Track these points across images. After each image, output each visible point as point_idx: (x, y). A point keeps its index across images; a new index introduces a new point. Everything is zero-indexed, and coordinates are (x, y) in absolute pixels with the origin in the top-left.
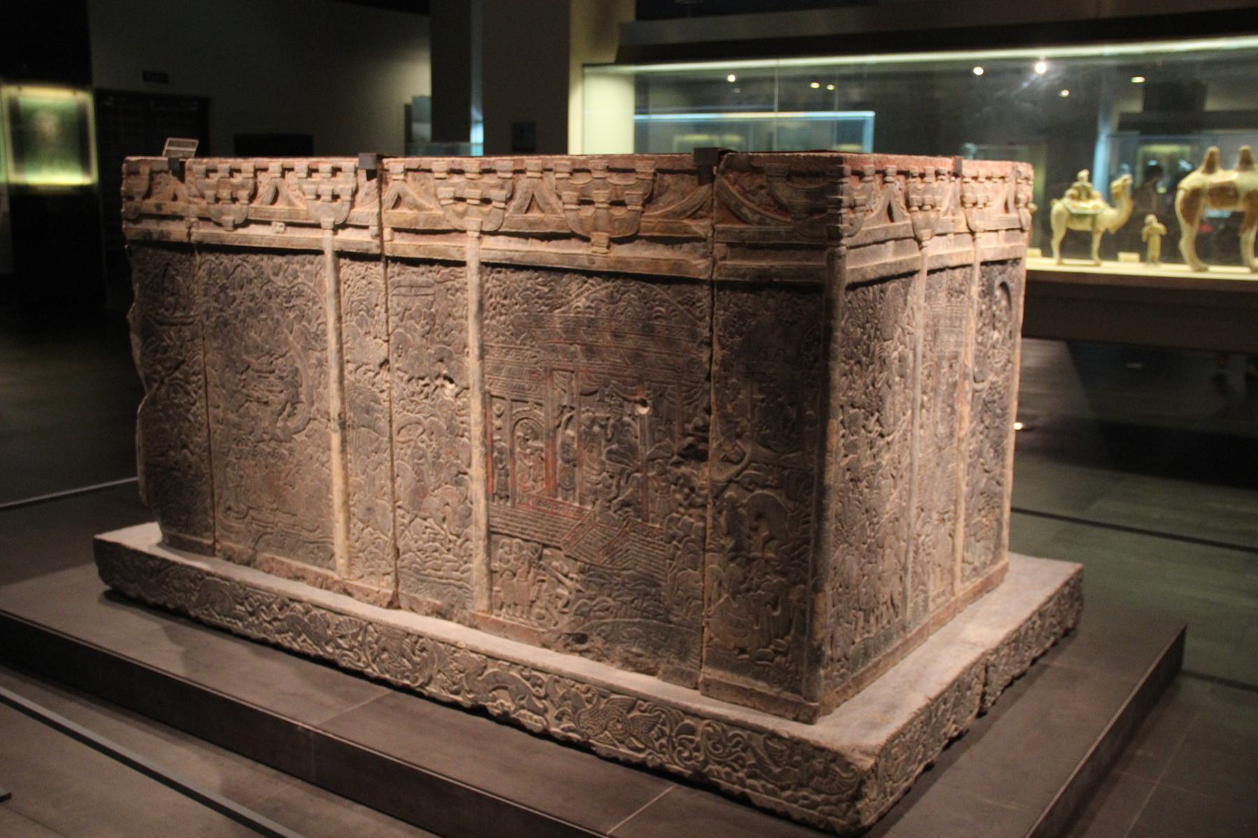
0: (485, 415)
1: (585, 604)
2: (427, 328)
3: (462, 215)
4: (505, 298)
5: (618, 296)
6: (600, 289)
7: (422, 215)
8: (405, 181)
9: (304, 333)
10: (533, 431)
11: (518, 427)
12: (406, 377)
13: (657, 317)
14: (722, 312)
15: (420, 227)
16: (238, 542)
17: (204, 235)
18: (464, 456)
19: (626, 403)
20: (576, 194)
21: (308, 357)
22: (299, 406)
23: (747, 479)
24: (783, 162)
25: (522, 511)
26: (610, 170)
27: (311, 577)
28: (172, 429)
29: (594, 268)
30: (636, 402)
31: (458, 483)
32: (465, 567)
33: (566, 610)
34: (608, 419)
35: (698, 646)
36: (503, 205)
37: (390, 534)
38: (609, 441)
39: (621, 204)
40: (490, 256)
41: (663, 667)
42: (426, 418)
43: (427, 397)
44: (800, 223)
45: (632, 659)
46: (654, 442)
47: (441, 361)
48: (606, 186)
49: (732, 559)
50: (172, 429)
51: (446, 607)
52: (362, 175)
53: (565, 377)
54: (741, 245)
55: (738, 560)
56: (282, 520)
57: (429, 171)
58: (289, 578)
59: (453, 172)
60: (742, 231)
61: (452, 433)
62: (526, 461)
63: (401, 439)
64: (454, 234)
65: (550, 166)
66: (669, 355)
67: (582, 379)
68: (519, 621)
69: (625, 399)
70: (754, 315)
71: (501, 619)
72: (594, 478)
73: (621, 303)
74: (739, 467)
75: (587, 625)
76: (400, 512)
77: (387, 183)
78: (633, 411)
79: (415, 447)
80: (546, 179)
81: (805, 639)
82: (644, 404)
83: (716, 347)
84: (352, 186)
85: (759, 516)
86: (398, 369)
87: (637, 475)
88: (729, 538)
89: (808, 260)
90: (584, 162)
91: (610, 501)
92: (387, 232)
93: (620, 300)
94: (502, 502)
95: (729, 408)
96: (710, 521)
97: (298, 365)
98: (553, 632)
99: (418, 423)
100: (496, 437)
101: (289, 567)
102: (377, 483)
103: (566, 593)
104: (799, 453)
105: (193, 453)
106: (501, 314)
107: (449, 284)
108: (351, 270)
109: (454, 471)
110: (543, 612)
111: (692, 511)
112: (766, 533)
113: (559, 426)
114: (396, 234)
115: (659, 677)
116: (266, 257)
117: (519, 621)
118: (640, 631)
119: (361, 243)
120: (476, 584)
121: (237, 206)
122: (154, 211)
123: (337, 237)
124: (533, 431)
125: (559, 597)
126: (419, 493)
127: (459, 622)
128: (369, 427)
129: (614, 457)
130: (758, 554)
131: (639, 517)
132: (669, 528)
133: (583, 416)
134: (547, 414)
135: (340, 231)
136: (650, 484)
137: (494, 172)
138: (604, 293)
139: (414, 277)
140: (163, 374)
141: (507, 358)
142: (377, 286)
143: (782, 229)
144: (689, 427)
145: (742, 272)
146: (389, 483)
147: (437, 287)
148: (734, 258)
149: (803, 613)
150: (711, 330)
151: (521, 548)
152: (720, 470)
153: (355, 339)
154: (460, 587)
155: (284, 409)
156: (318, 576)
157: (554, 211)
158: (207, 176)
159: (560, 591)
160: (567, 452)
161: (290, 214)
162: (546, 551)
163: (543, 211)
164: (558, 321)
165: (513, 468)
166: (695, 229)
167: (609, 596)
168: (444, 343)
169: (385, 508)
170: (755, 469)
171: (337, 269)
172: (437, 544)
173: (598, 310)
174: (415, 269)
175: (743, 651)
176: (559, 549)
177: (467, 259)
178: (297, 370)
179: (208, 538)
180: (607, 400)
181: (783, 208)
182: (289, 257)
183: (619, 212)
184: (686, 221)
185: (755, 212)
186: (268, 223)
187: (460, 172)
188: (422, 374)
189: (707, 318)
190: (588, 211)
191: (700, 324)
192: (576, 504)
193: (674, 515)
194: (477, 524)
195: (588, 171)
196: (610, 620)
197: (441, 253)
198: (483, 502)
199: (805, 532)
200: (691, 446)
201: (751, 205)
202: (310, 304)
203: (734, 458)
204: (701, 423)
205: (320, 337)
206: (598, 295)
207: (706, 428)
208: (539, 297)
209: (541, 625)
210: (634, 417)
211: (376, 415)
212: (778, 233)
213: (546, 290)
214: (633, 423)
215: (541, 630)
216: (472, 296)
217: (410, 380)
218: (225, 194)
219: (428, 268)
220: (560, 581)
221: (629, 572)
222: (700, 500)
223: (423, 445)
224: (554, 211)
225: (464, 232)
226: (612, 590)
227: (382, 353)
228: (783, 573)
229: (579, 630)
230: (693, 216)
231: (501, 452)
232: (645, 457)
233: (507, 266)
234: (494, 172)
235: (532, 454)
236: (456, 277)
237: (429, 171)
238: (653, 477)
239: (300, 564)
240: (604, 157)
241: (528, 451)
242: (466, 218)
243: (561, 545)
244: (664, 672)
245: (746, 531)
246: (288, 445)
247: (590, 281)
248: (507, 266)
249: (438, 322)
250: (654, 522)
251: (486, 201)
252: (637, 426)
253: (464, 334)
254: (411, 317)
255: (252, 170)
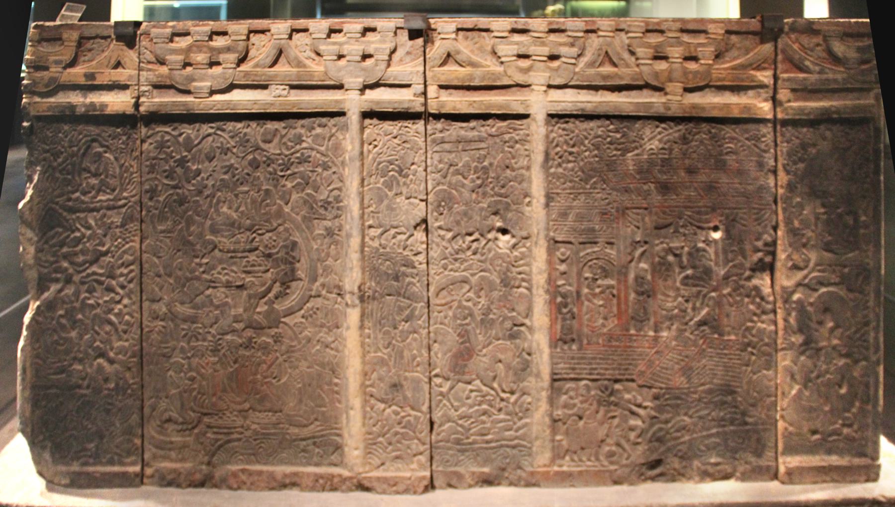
0: (549, 262)
1: (661, 429)
2: (479, 182)
3: (527, 71)
4: (573, 146)
5: (691, 137)
6: (674, 132)
7: (478, 72)
8: (456, 39)
9: (310, 203)
10: (604, 270)
11: (586, 268)
12: (449, 235)
13: (727, 153)
14: (785, 144)
15: (476, 83)
16: (183, 460)
17: (161, 104)
18: (521, 308)
19: (699, 231)
20: (652, 51)
21: (310, 229)
22: (294, 284)
23: (814, 281)
24: (838, 26)
25: (589, 353)
26: (683, 31)
27: (306, 481)
28: (81, 337)
29: (670, 113)
30: (709, 228)
31: (513, 337)
32: (519, 424)
33: (639, 440)
34: (682, 248)
35: (773, 440)
36: (573, 61)
37: (425, 408)
38: (683, 268)
39: (695, 59)
40: (559, 108)
41: (741, 469)
42: (473, 275)
43: (474, 253)
44: (852, 71)
45: (710, 469)
46: (727, 261)
47: (496, 213)
48: (680, 43)
49: (802, 353)
50: (81, 337)
51: (495, 472)
52: (404, 36)
53: (638, 214)
54: (802, 90)
55: (808, 353)
56: (259, 420)
57: (487, 30)
58: (272, 489)
59: (514, 31)
60: (805, 79)
61: (505, 286)
62: (595, 301)
63: (438, 302)
64: (514, 89)
65: (623, 26)
66: (740, 184)
67: (656, 214)
68: (589, 465)
69: (699, 227)
70: (814, 145)
71: (565, 468)
72: (669, 305)
73: (694, 143)
74: (805, 272)
75: (662, 449)
76: (438, 381)
77: (433, 43)
78: (707, 236)
79: (459, 307)
80: (617, 38)
81: (870, 407)
82: (716, 229)
83: (781, 174)
84: (389, 46)
85: (826, 310)
86: (440, 228)
87: (713, 294)
88: (798, 336)
89: (859, 99)
90: (658, 24)
91: (686, 324)
92: (432, 91)
93: (692, 141)
94: (566, 347)
95: (796, 224)
96: (781, 323)
97: (297, 237)
98: (626, 466)
99: (465, 281)
100: (560, 282)
101: (272, 476)
102: (406, 353)
103: (639, 423)
104: (857, 252)
105: (111, 362)
106: (569, 162)
107: (507, 137)
108: (375, 128)
109: (508, 324)
110: (614, 448)
111: (764, 317)
112: (831, 324)
113: (631, 261)
114: (443, 91)
115: (737, 479)
116: (254, 124)
117: (589, 465)
118: (718, 440)
119: (400, 102)
120: (537, 438)
121: (216, 70)
122: (82, 81)
123: (363, 97)
124: (604, 270)
125: (632, 429)
126: (463, 357)
127: (511, 484)
128: (399, 294)
129: (691, 281)
130: (824, 344)
131: (715, 332)
132: (744, 336)
133: (658, 248)
134: (618, 251)
135: (368, 91)
136: (725, 300)
137: (563, 31)
138: (676, 135)
139: (463, 132)
140: (71, 271)
141: (575, 203)
142: (416, 143)
143: (839, 77)
144: (760, 244)
145: (806, 112)
146: (425, 353)
147: (490, 141)
148: (796, 100)
149: (867, 385)
150: (776, 160)
151: (588, 388)
152: (788, 277)
153: (381, 201)
154: (514, 447)
155: (269, 290)
156: (317, 477)
157: (627, 66)
158: (172, 41)
159: (633, 422)
160: (641, 285)
161: (299, 76)
162: (617, 386)
163: (615, 65)
164: (630, 162)
165: (580, 310)
166: (761, 78)
167: (686, 414)
168: (501, 195)
169: (419, 381)
170: (819, 271)
171: (362, 129)
172: (485, 406)
173: (671, 150)
174: (464, 125)
175: (814, 432)
176: (633, 380)
177: (531, 111)
178: (295, 244)
179: (133, 464)
180: (682, 230)
181: (836, 59)
182: (291, 122)
183: (692, 66)
184: (752, 72)
185: (817, 64)
186: (265, 87)
187: (524, 31)
188: (471, 230)
189: (772, 151)
190: (662, 66)
191: (767, 155)
192: (651, 333)
193: (749, 324)
194: (538, 375)
195: (662, 32)
196: (687, 438)
197: (501, 107)
198: (546, 350)
199: (865, 316)
200: (761, 260)
201: (811, 59)
202: (319, 170)
203: (802, 264)
204: (769, 239)
205: (334, 205)
206: (671, 137)
207: (774, 243)
208: (610, 143)
209: (612, 463)
210: (707, 242)
211: (408, 280)
212: (835, 81)
213: (618, 136)
214: (708, 248)
215: (612, 467)
216: (538, 147)
217: (454, 237)
218: (201, 57)
219: (481, 122)
220: (633, 413)
221: (707, 386)
222: (770, 307)
223: (470, 304)
224: (627, 66)
225: (529, 86)
226: (689, 408)
227: (420, 211)
228: (847, 355)
229: (655, 457)
230: (759, 68)
231: (564, 296)
232: (720, 278)
233: (576, 117)
234: (563, 31)
235: (602, 292)
236: (515, 130)
237: (487, 30)
238: (730, 294)
239: (289, 469)
240: (675, 20)
241: (597, 290)
242: (531, 73)
243: (634, 377)
244: (743, 474)
245: (814, 325)
246: (273, 331)
247: (663, 125)
248: (576, 117)
249: (492, 175)
250: (729, 334)
251: (553, 57)
252: (711, 250)
253: (525, 185)
254: (457, 172)
255: (246, 32)
